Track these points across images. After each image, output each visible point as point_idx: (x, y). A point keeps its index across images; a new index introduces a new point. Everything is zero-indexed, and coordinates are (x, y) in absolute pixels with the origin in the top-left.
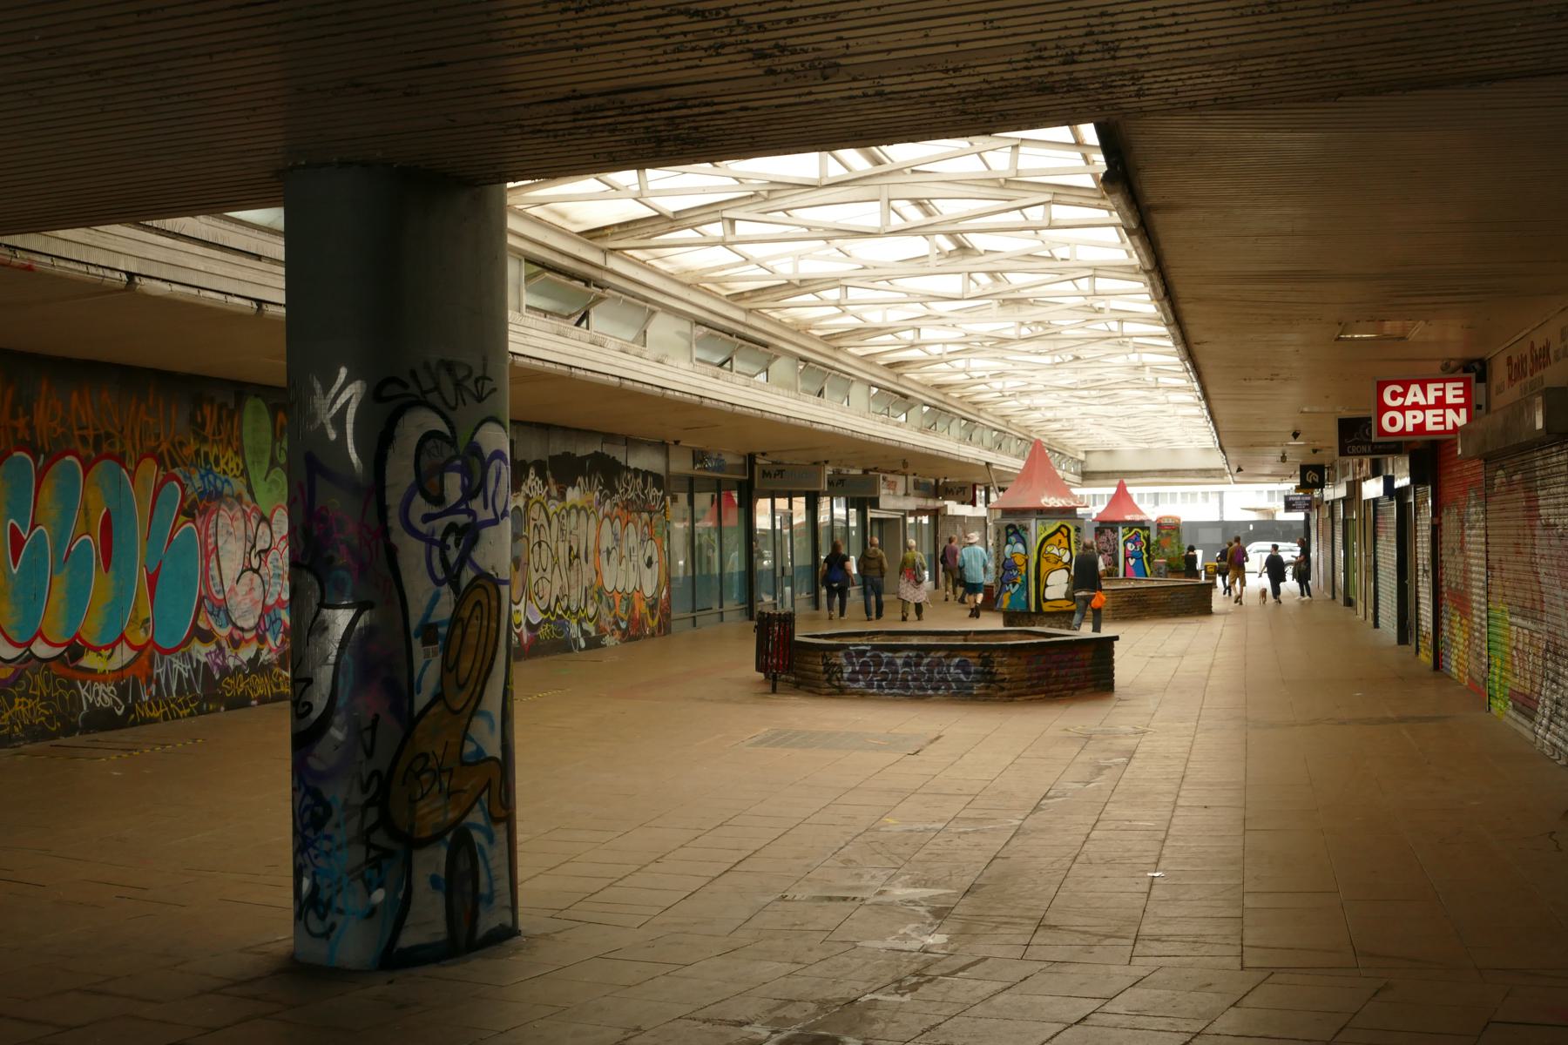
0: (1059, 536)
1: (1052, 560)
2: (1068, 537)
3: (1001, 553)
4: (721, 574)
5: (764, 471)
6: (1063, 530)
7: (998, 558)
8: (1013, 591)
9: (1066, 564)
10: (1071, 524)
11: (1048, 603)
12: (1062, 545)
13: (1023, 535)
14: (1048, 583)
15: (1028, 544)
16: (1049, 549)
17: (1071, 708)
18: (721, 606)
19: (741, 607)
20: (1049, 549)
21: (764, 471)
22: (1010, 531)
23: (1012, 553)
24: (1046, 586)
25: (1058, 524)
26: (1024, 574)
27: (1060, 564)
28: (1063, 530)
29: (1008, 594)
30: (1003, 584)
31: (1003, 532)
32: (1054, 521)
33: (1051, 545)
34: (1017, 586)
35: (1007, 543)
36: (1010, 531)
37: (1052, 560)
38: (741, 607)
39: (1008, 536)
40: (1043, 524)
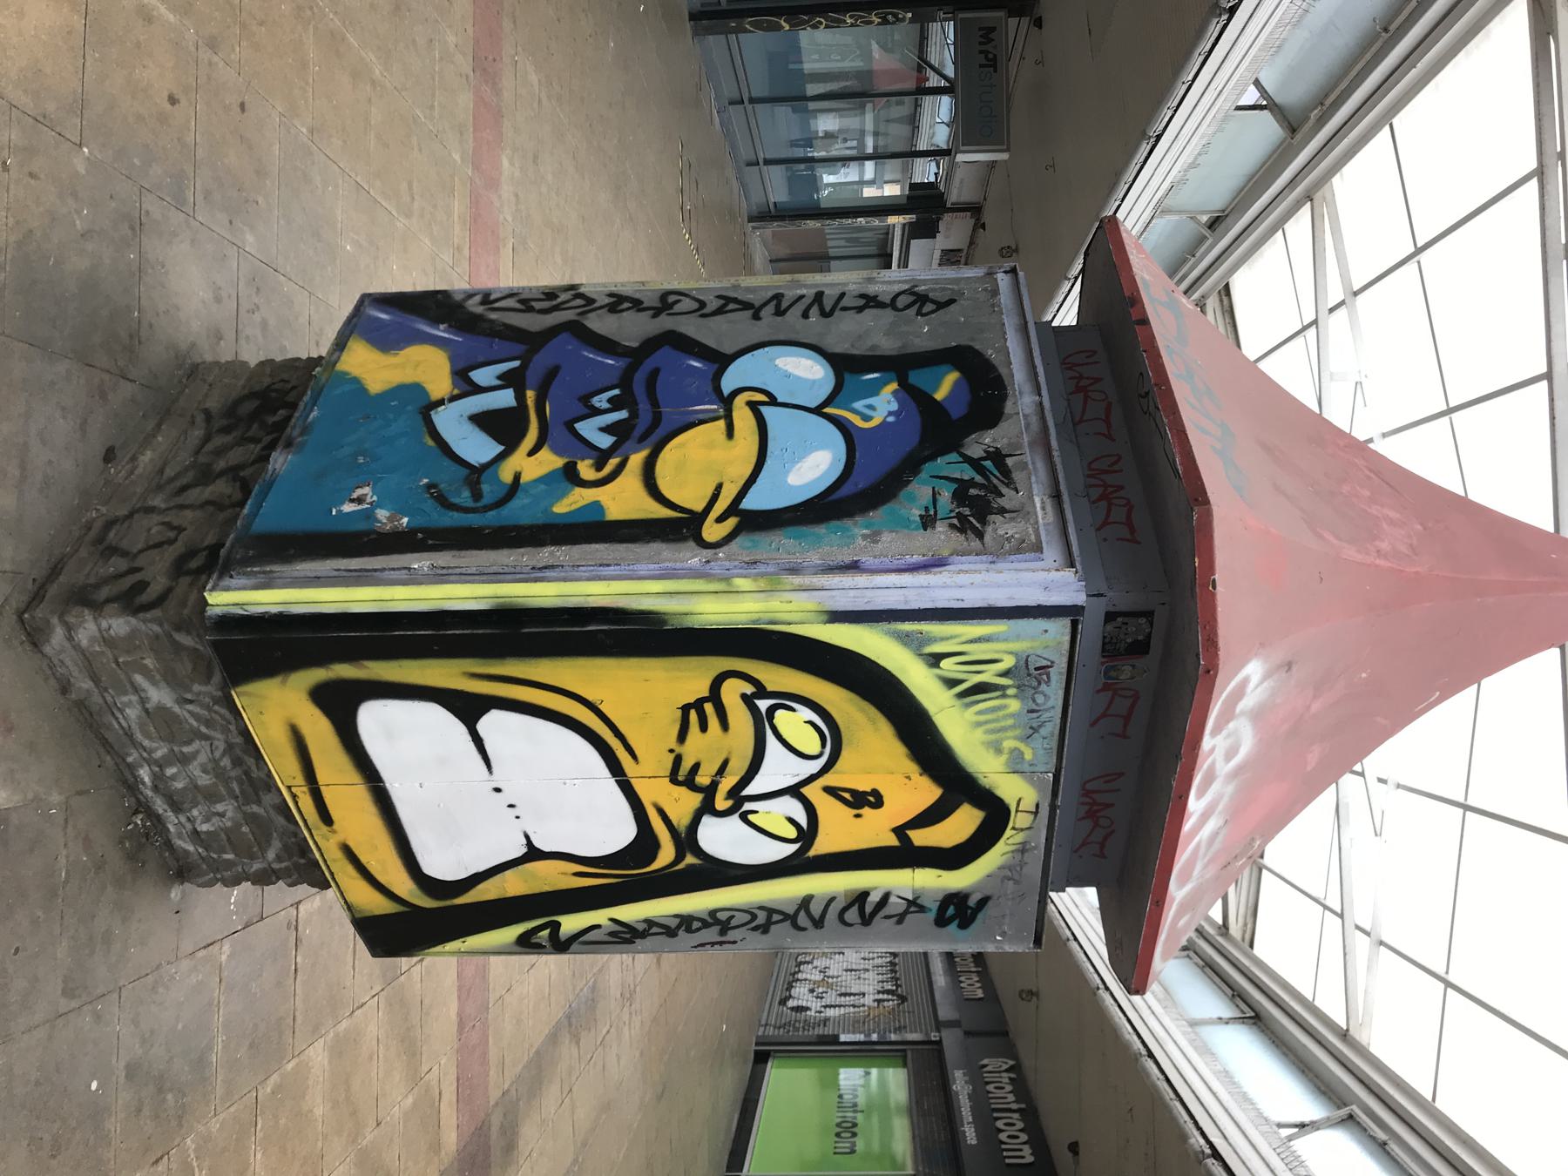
0: (916, 792)
1: (703, 748)
2: (902, 855)
3: (768, 324)
4: (813, 160)
5: (993, 29)
6: (963, 823)
7: (728, 303)
8: (453, 424)
9: (687, 840)
10: (1008, 873)
11: (319, 730)
12: (828, 810)
13: (920, 491)
14: (493, 724)
15: (830, 541)
16: (795, 724)
17: (564, 659)
18: (768, 162)
19: (772, 206)
20: (795, 724)
21: (993, 29)
22: (946, 385)
23: (764, 401)
24: (468, 709)
25: (1015, 790)
26: (572, 501)
27: (682, 804)
28: (963, 823)
29: (439, 382)
30: (532, 342)
31: (924, 334)
32: (1038, 753)
33: (833, 736)
34: (477, 447)
35: (844, 365)
36: (946, 385)
37: (703, 748)
38: (772, 206)
39: (899, 366)
40: (1028, 674)
